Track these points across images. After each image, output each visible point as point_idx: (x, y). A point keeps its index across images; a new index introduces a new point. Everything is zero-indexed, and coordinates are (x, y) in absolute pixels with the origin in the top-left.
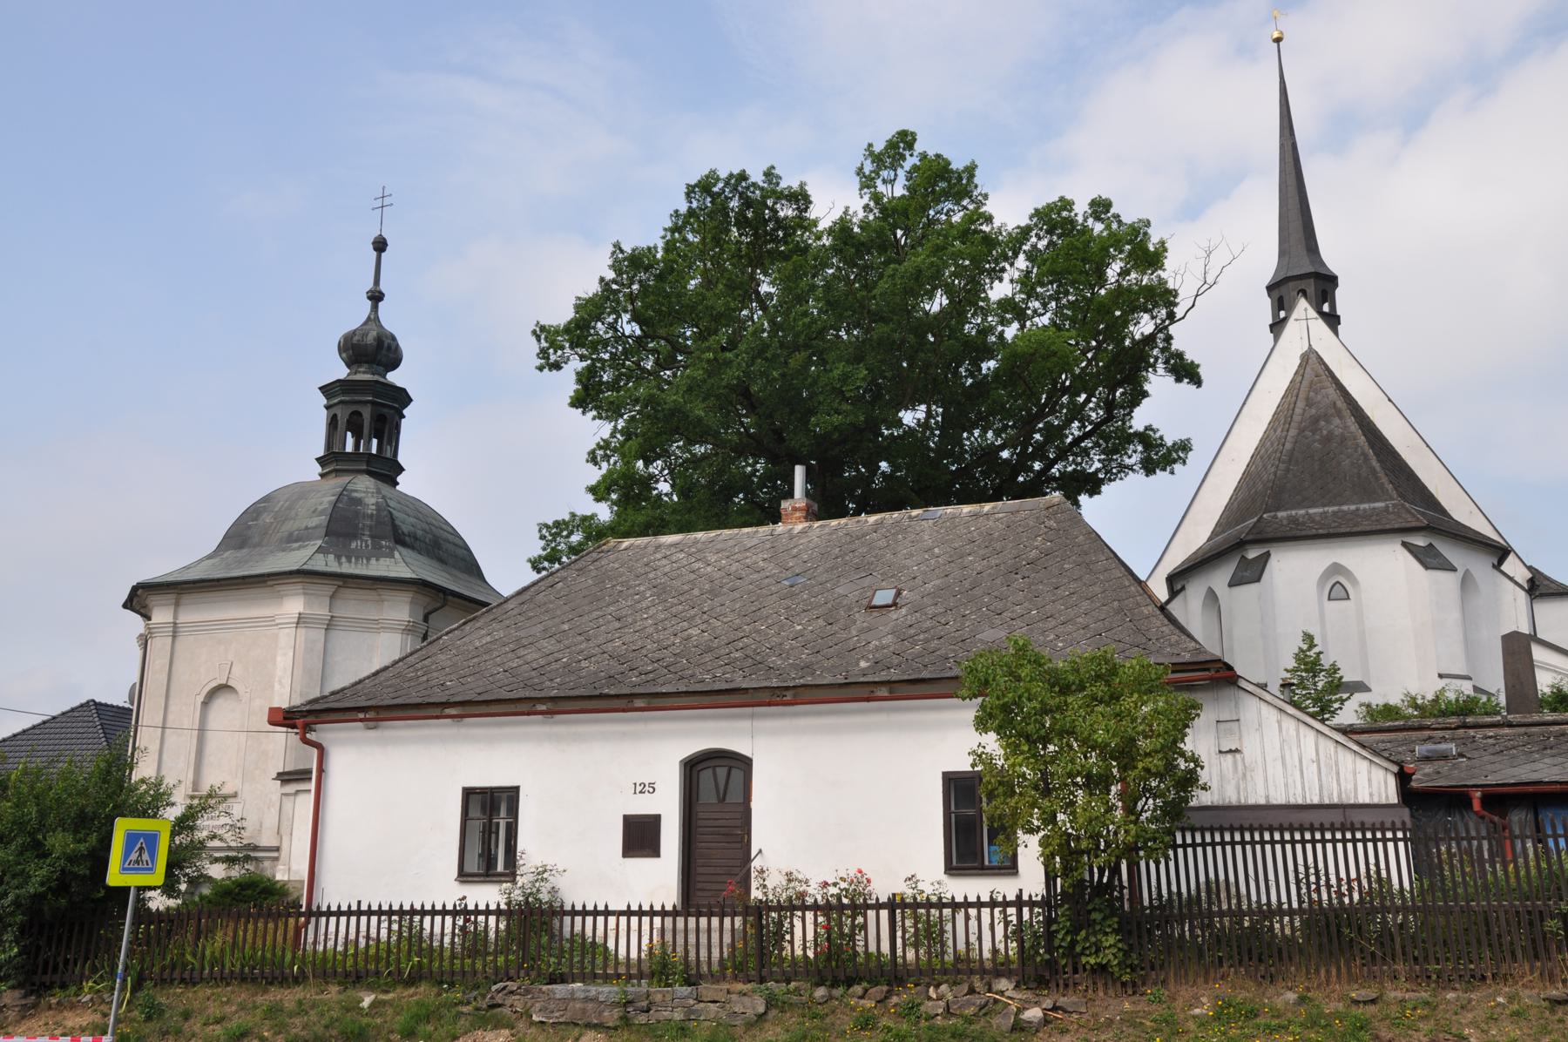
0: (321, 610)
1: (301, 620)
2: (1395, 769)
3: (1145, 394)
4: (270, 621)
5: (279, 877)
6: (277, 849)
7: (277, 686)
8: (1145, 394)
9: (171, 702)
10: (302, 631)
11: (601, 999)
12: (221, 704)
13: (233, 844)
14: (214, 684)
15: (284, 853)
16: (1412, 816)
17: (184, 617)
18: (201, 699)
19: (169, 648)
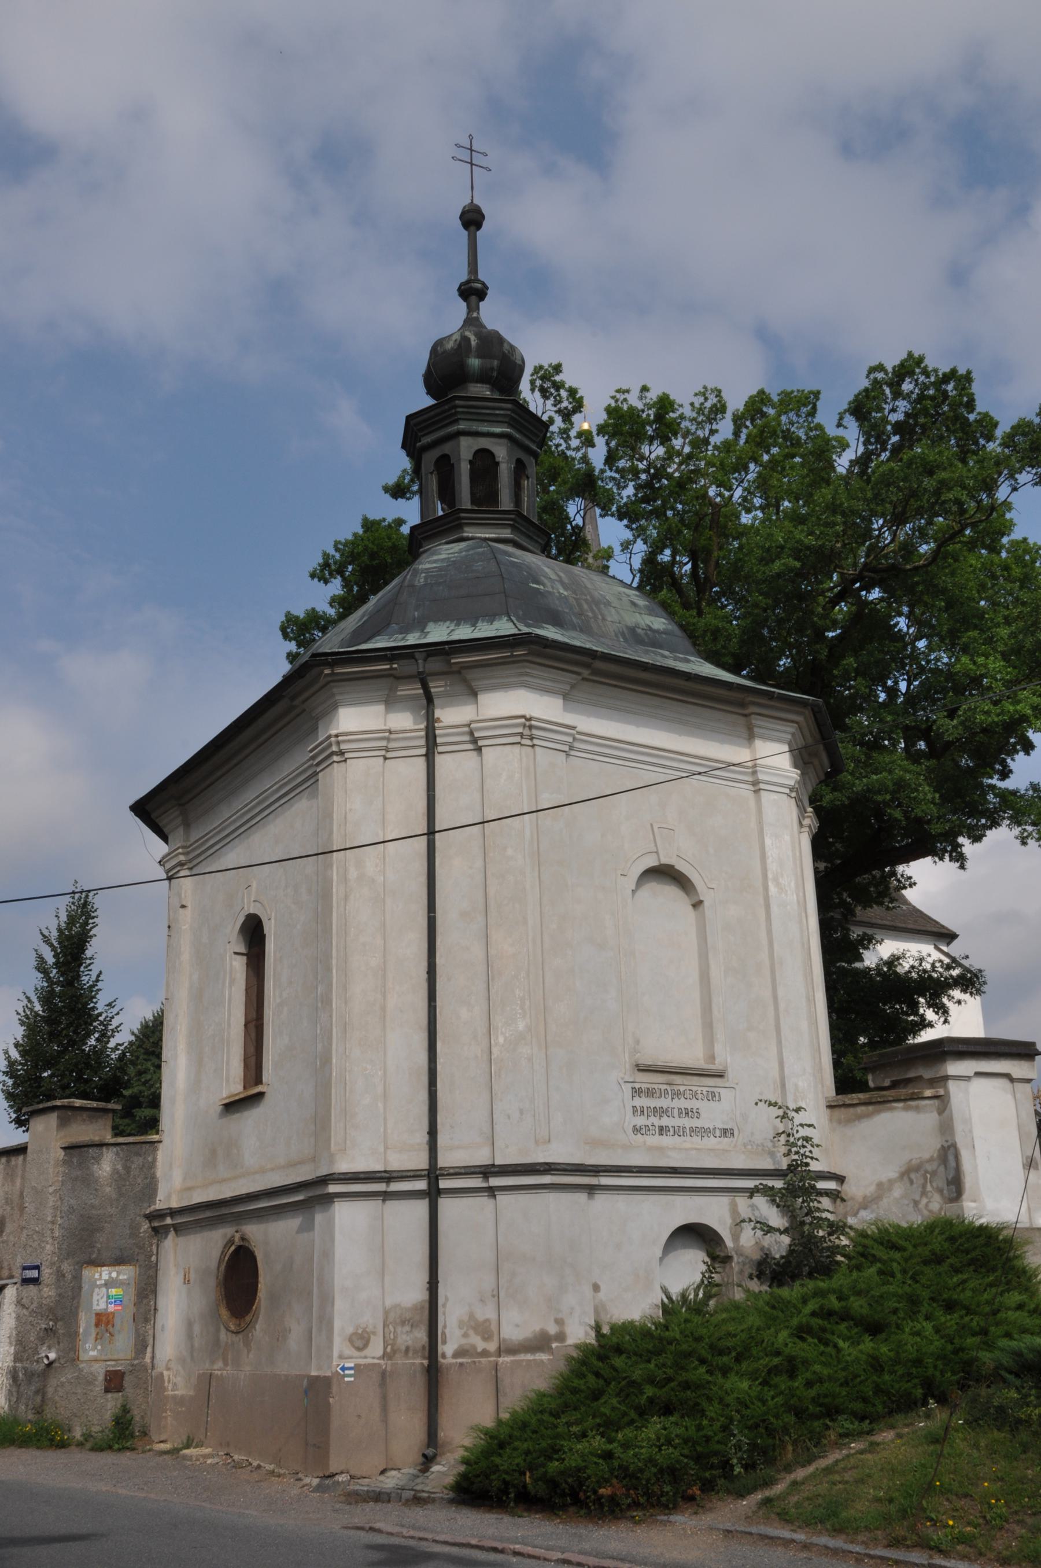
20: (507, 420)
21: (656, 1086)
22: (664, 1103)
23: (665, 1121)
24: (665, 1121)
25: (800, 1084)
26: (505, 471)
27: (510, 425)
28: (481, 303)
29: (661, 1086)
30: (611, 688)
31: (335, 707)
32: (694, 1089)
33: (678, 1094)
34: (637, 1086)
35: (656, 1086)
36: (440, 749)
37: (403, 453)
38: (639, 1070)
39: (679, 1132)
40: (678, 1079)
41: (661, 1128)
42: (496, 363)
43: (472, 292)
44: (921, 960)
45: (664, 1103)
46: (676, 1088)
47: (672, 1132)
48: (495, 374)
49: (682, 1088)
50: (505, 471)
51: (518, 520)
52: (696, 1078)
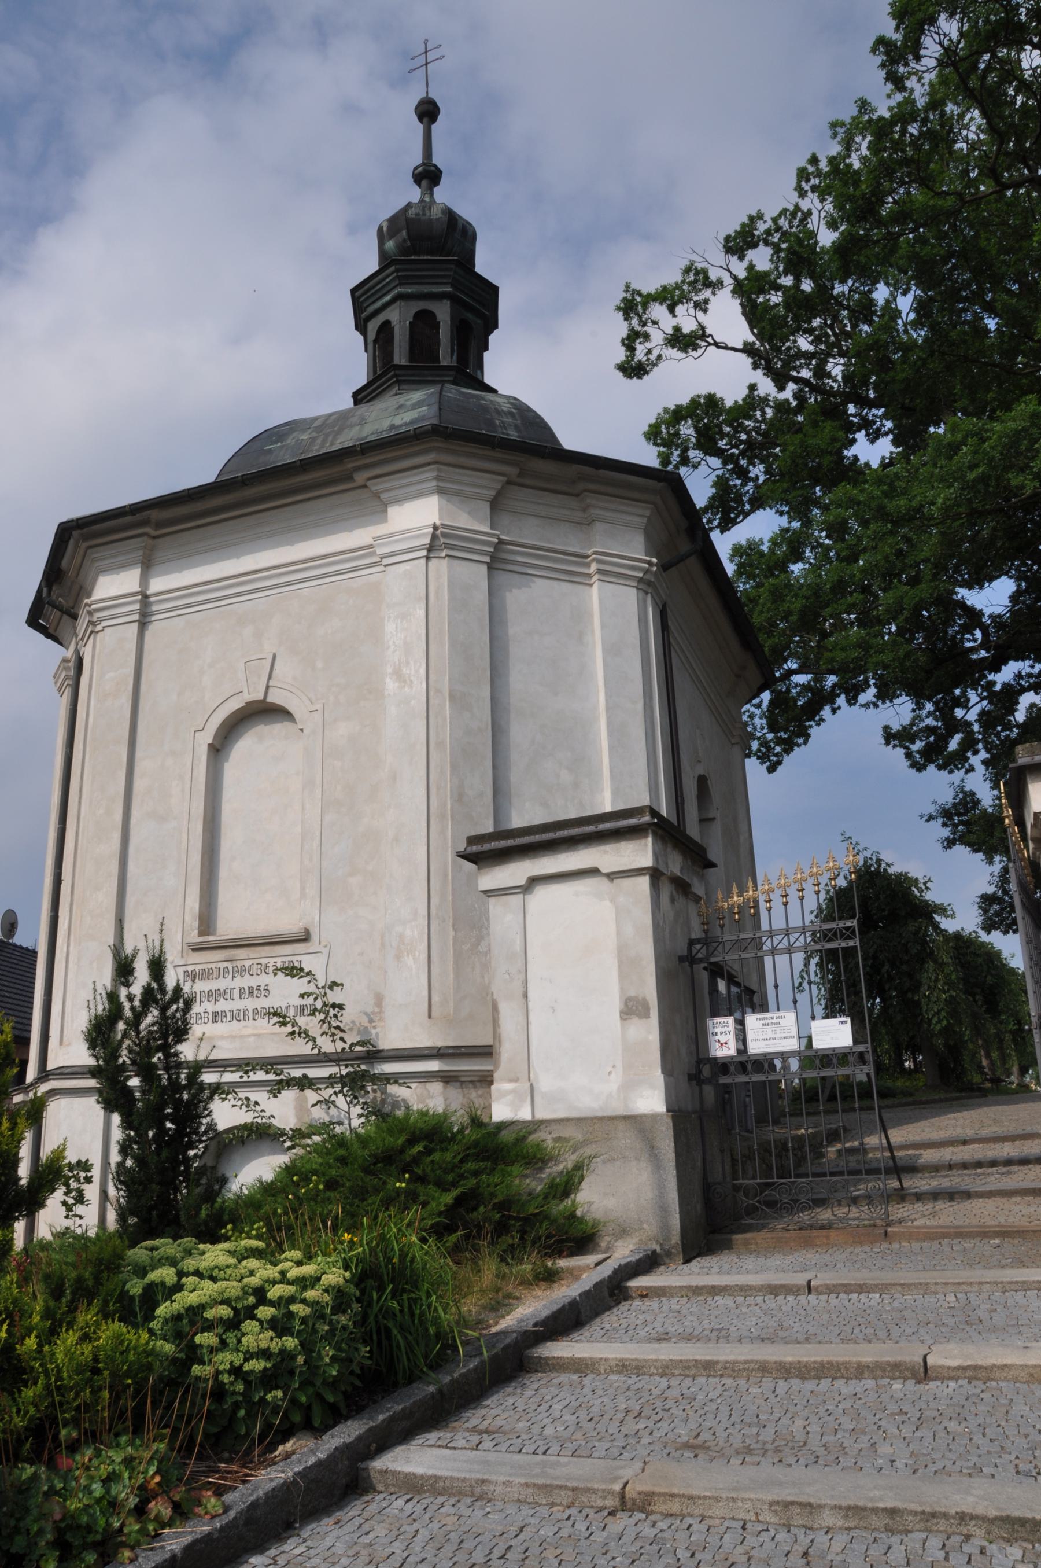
0: (472, 520)
1: (439, 543)
2: (697, 933)
3: (795, 189)
4: (367, 558)
5: (500, 1112)
6: (486, 1052)
7: (391, 685)
8: (795, 189)
9: (139, 753)
10: (440, 567)
11: (468, 1500)
12: (251, 746)
13: (327, 1046)
14: (236, 704)
15: (507, 1052)
16: (18, 1147)
17: (158, 584)
18: (207, 737)
19: (132, 646)
20: (397, 282)
21: (213, 966)
22: (221, 984)
23: (222, 1005)
24: (222, 1005)
25: (408, 932)
26: (444, 333)
27: (400, 284)
28: (435, 189)
29: (220, 965)
30: (194, 531)
31: (95, 581)
32: (264, 961)
33: (241, 971)
34: (190, 968)
35: (213, 966)
36: (154, 608)
37: (358, 333)
38: (193, 950)
39: (237, 1016)
40: (241, 953)
41: (216, 1014)
42: (404, 233)
43: (428, 176)
44: (834, 711)
45: (221, 984)
46: (239, 964)
47: (229, 1018)
48: (409, 244)
49: (247, 963)
50: (444, 333)
51: (398, 372)
52: (267, 948)
